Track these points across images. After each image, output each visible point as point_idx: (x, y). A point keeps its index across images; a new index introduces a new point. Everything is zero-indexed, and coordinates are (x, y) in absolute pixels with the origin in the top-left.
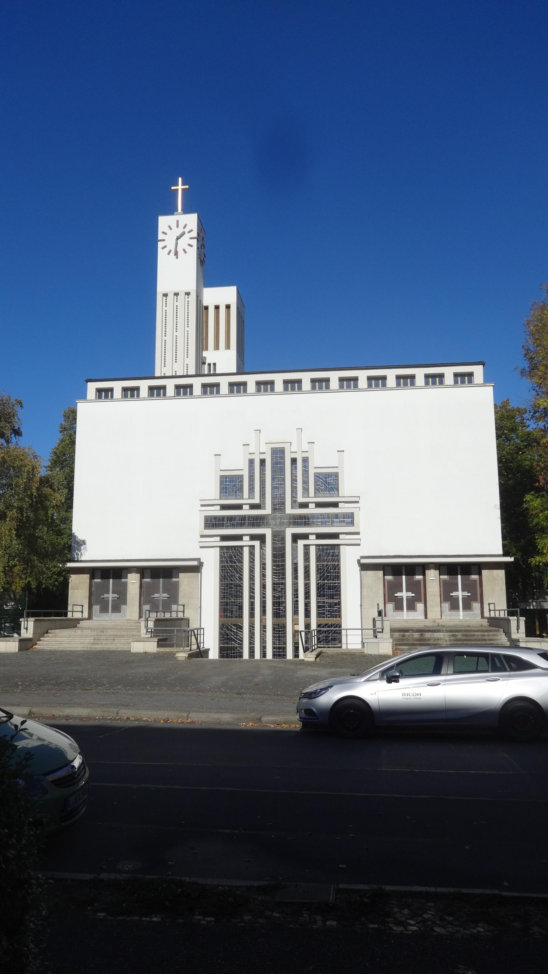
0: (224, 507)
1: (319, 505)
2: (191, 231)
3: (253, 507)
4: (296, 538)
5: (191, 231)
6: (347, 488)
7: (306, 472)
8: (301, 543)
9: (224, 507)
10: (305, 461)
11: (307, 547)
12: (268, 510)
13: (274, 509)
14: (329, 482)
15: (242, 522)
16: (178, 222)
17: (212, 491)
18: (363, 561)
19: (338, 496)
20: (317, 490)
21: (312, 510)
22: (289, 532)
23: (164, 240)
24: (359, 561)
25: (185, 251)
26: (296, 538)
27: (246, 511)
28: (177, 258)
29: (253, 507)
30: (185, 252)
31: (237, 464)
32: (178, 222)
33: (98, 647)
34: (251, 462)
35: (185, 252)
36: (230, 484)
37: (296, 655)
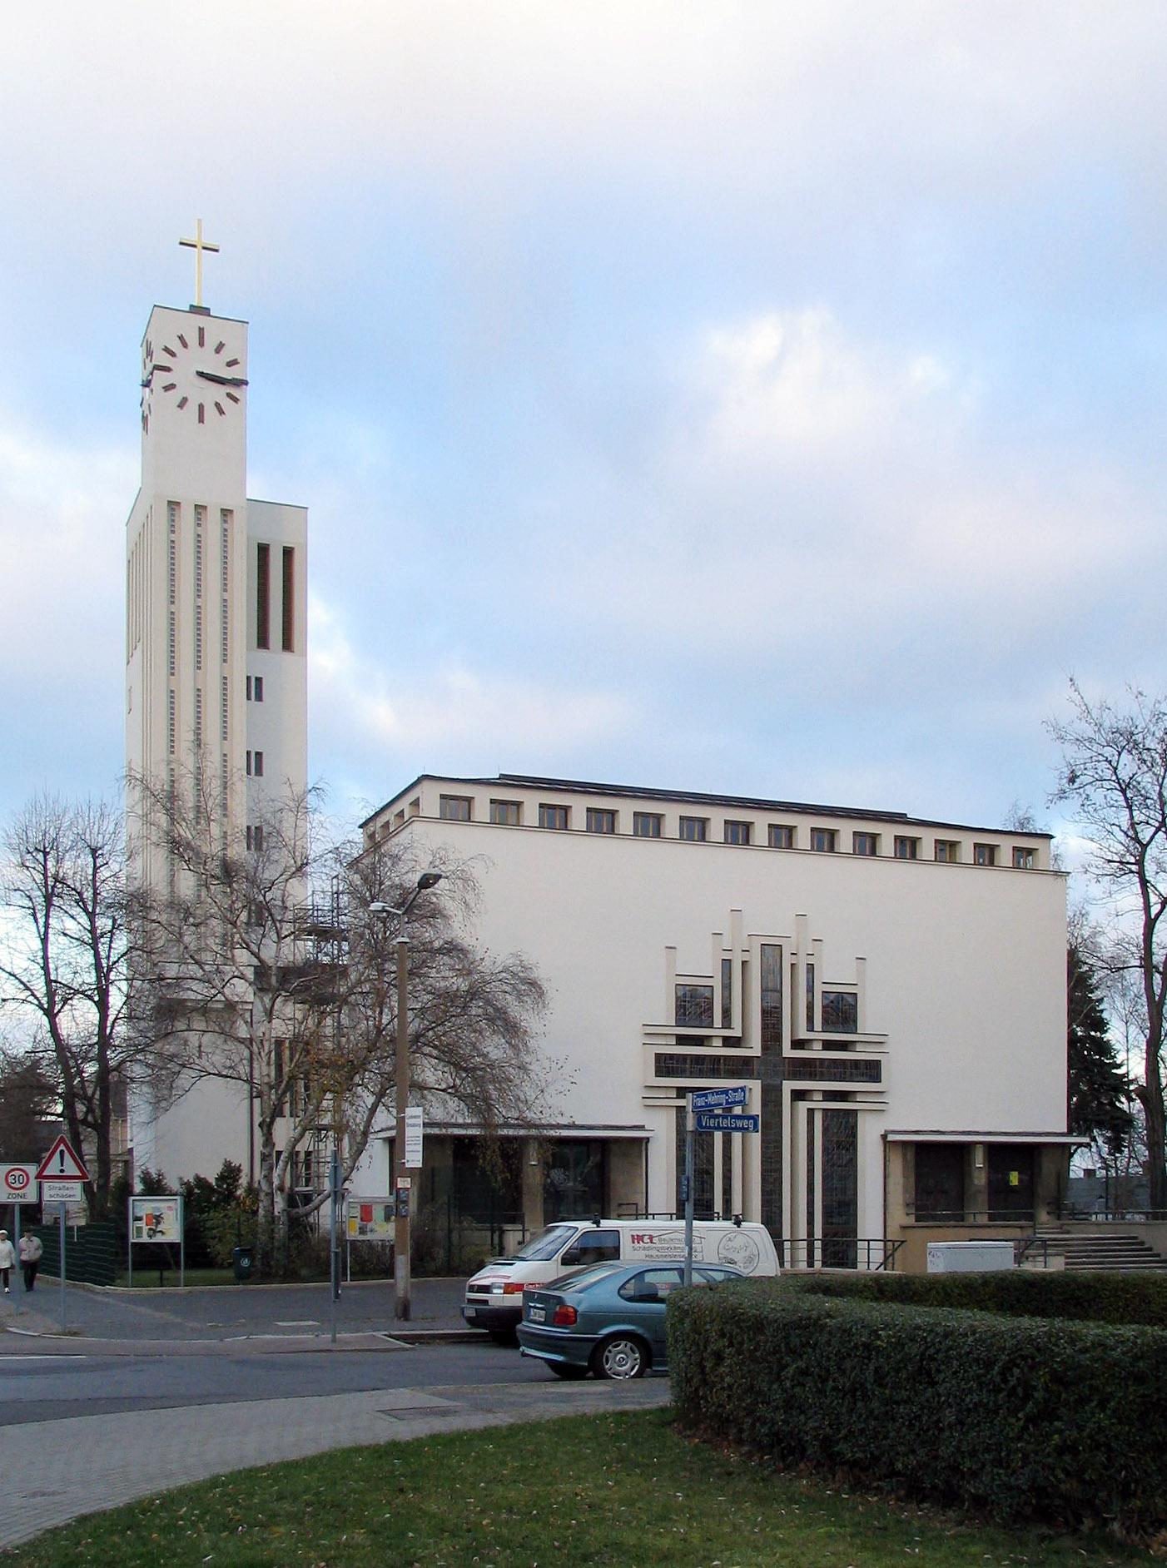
0: (682, 1040)
1: (828, 1045)
2: (168, 388)
3: (728, 1042)
4: (799, 1095)
5: (168, 388)
6: (869, 1020)
7: (810, 990)
8: (803, 1106)
9: (682, 1040)
10: (811, 968)
11: (811, 1112)
12: (754, 1049)
13: (765, 1048)
14: (841, 1011)
15: (713, 1067)
16: (201, 330)
17: (663, 1012)
18: (891, 1138)
19: (855, 1032)
20: (825, 1021)
21: (816, 1053)
22: (788, 1086)
23: (167, 369)
24: (884, 1137)
25: (183, 403)
26: (799, 1095)
27: (716, 1050)
28: (201, 374)
29: (728, 1042)
30: (181, 405)
31: (702, 966)
32: (201, 330)
33: (1144, 1047)
34: (727, 963)
35: (181, 405)
36: (692, 1005)
37: (811, 1264)
